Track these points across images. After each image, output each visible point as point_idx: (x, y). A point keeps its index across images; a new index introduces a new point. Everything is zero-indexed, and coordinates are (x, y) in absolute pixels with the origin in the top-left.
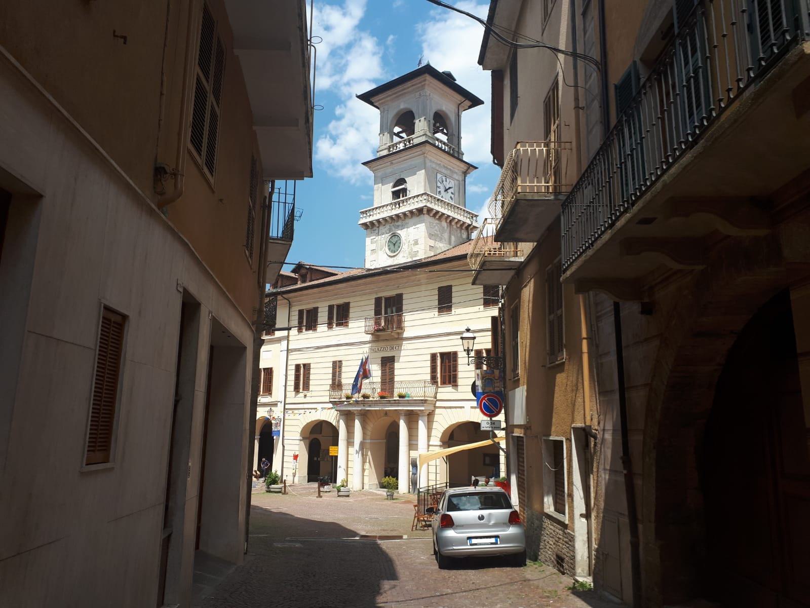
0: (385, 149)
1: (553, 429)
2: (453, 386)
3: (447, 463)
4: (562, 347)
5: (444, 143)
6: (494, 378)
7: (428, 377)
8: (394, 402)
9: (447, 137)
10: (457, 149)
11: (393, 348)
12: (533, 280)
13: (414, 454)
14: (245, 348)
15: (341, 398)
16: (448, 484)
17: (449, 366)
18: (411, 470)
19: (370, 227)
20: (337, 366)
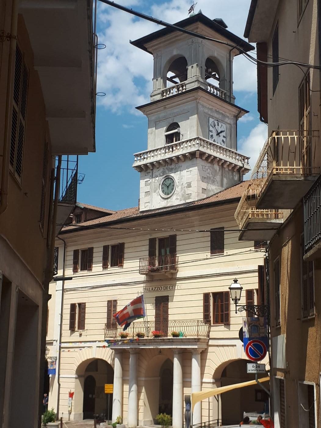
0: (159, 94)
1: (307, 375)
2: (225, 325)
3: (218, 401)
4: (313, 306)
5: (216, 88)
6: (259, 324)
7: (201, 316)
8: (168, 340)
9: (219, 82)
10: (228, 94)
11: (167, 288)
12: (290, 242)
13: (187, 391)
14: (38, 306)
15: (116, 337)
16: (220, 421)
17: (222, 305)
18: (185, 406)
19: (144, 169)
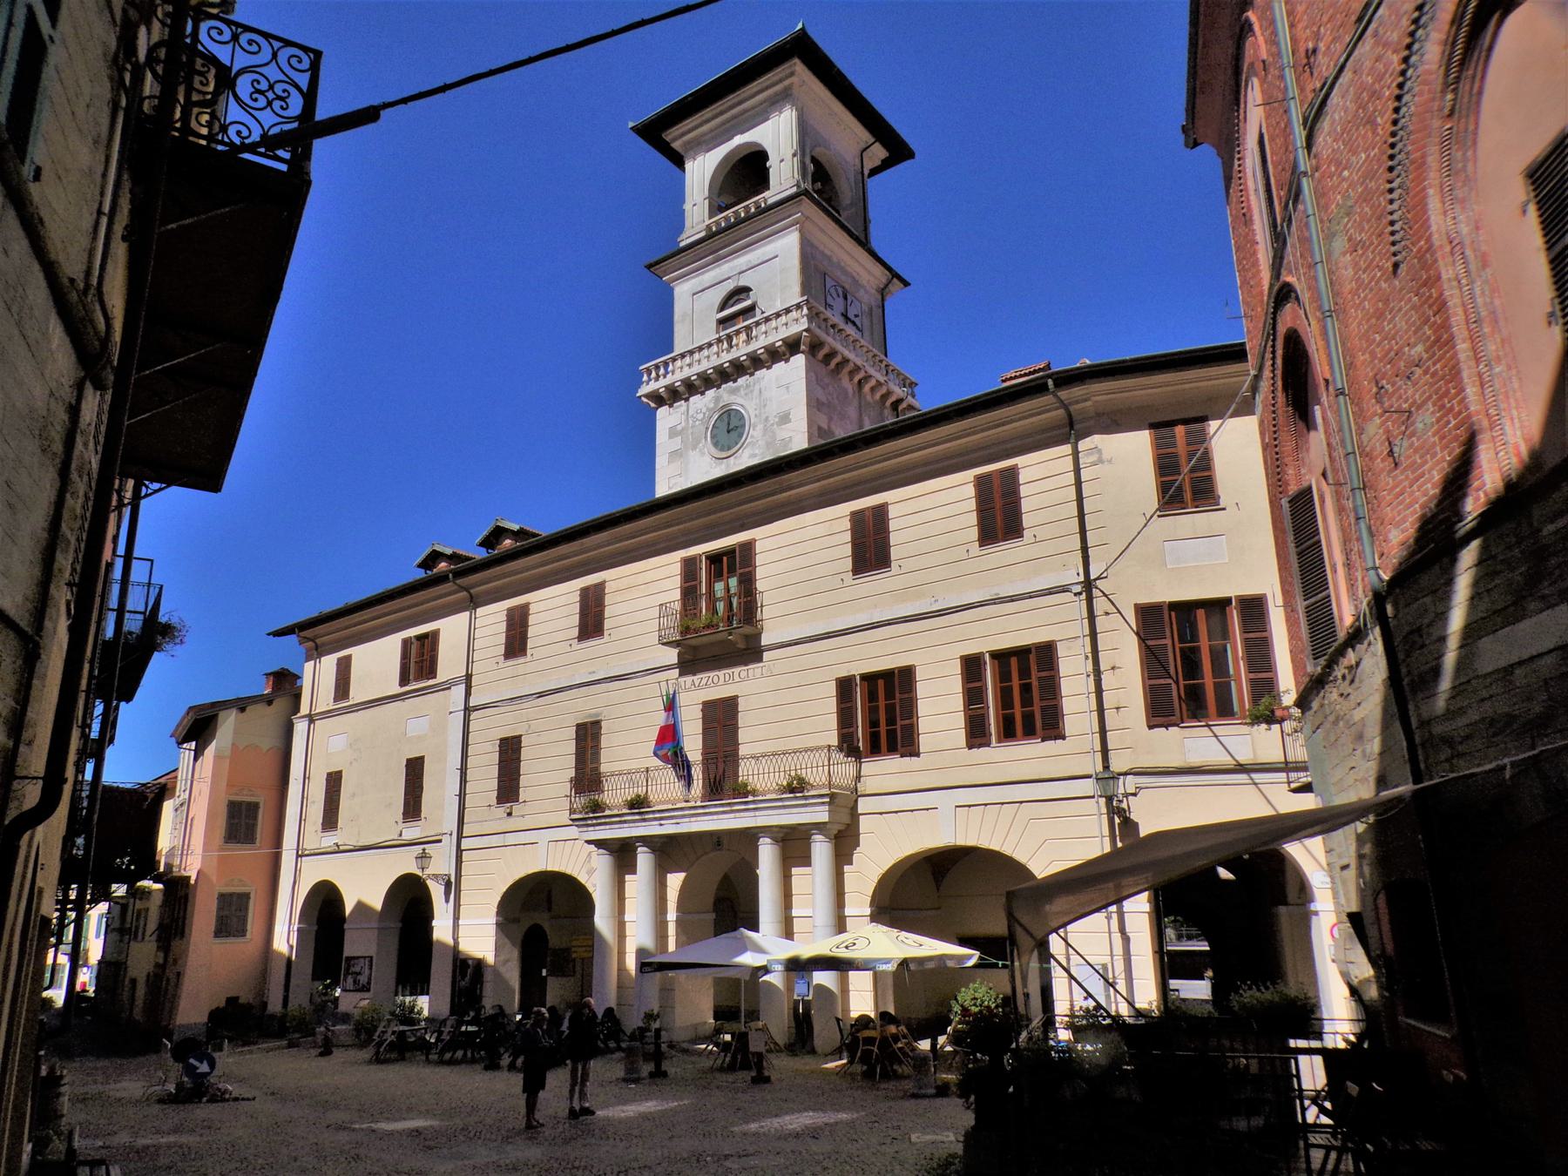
20: (588, 736)
